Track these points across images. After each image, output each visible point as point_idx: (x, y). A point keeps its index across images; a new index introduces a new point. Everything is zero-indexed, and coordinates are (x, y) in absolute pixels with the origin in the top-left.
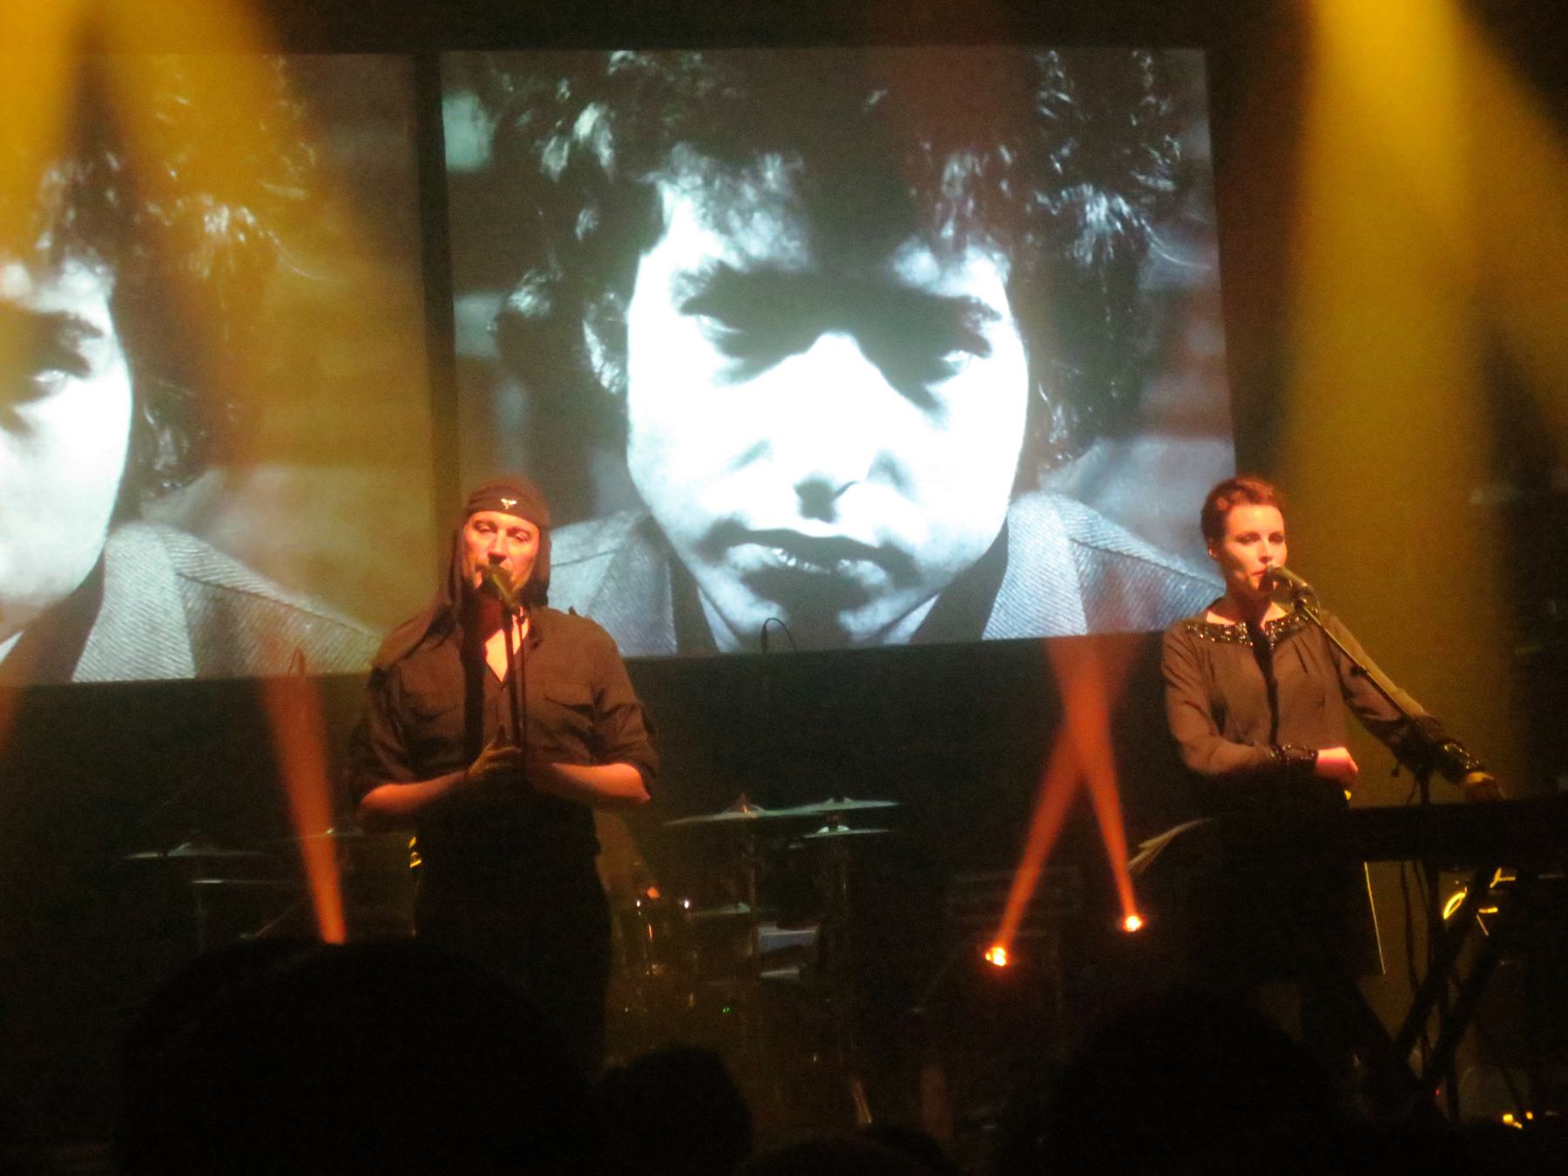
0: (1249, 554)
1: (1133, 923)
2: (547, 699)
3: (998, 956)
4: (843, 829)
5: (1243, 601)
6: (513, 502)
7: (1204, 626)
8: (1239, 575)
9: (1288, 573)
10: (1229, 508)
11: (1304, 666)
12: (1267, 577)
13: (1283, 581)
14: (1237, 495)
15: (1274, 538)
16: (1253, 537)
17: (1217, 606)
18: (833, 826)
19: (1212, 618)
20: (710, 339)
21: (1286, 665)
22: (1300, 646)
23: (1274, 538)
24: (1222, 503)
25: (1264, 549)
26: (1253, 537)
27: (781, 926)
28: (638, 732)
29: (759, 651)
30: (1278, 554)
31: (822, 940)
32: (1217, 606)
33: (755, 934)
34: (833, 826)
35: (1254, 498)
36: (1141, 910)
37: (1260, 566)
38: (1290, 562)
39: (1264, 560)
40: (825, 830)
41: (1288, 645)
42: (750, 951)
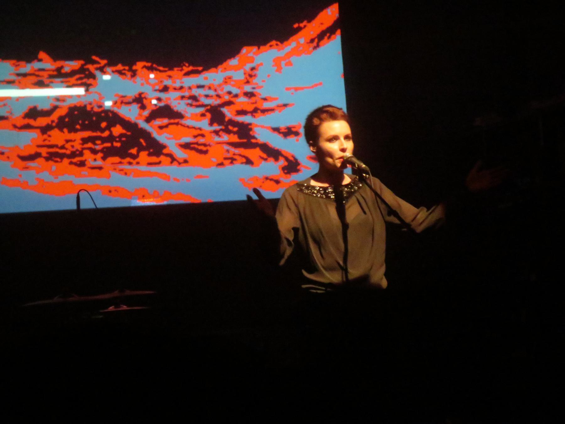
0: (334, 147)
4: (125, 307)
5: (329, 173)
7: (308, 187)
8: (330, 160)
9: (354, 160)
10: (320, 124)
11: (421, 223)
14: (324, 116)
15: (347, 137)
16: (334, 138)
17: (315, 177)
18: (117, 306)
19: (313, 183)
21: (353, 212)
22: (362, 201)
23: (347, 137)
24: (316, 121)
25: (342, 145)
26: (334, 138)
28: (289, 132)
30: (349, 145)
32: (315, 177)
34: (117, 306)
37: (342, 154)
38: (356, 152)
39: (343, 150)
40: (111, 308)
41: (353, 199)
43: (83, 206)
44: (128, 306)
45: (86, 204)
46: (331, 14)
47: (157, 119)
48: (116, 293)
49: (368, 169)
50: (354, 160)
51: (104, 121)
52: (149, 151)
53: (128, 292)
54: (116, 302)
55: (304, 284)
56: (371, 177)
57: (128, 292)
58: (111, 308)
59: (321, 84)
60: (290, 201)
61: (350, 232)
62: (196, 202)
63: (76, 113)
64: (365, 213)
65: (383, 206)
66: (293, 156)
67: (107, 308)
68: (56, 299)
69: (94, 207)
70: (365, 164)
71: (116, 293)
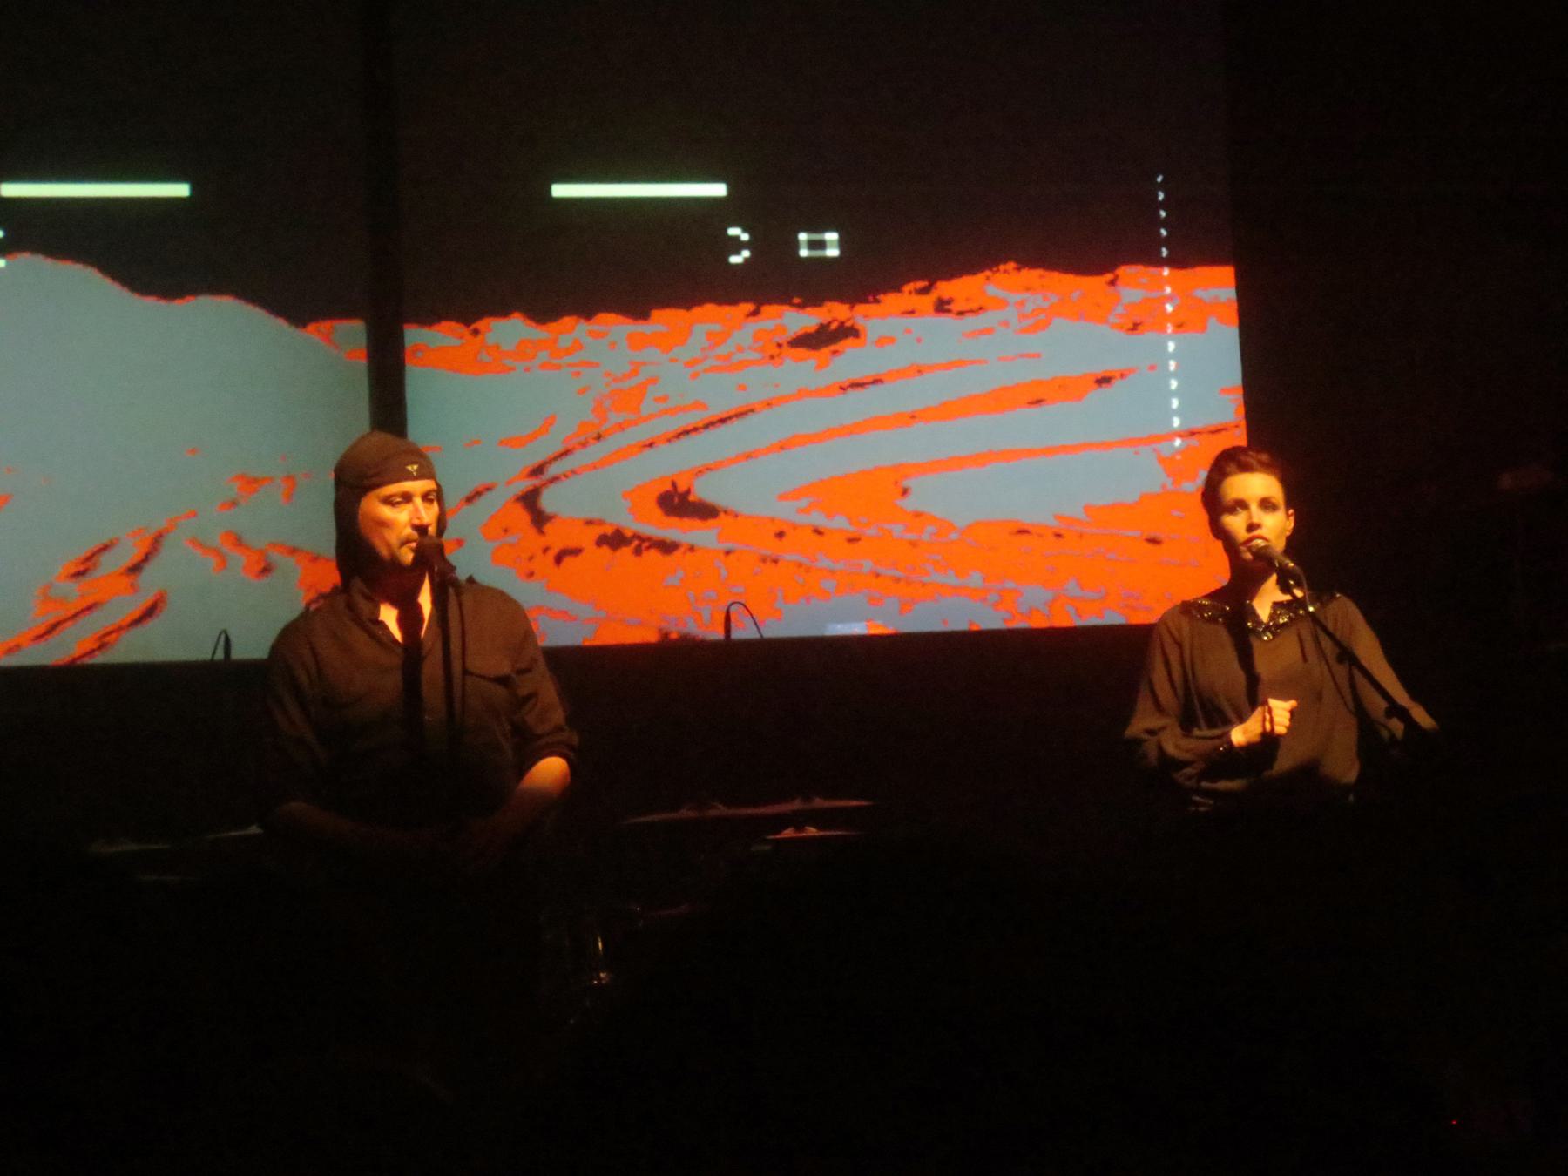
4: (811, 831)
18: (799, 828)
40: (789, 833)
43: (737, 634)
44: (820, 829)
45: (744, 631)
47: (445, 325)
48: (797, 805)
49: (1298, 570)
53: (819, 803)
54: (798, 820)
55: (1000, 725)
57: (819, 803)
58: (789, 833)
59: (1037, 356)
60: (1167, 639)
65: (1327, 644)
66: (1058, 517)
67: (779, 832)
68: (685, 813)
69: (757, 636)
71: (797, 805)
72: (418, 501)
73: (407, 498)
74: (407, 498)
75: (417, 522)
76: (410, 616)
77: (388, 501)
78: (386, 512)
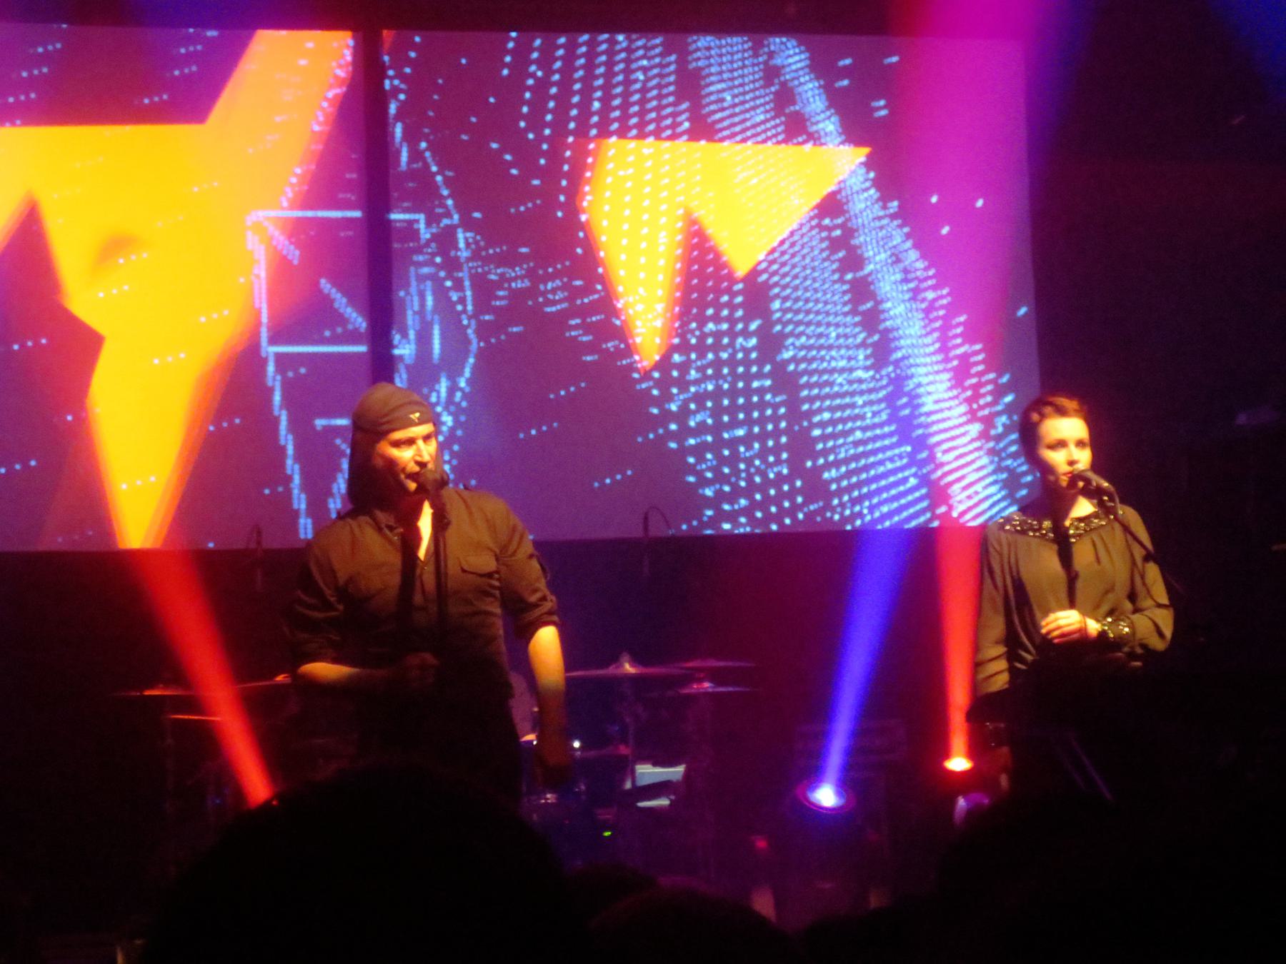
0: (1057, 458)
1: (826, 796)
2: (464, 571)
3: (826, 796)
6: (417, 415)
9: (1091, 475)
12: (1075, 477)
13: (1088, 481)
14: (1048, 410)
15: (1080, 444)
16: (1061, 444)
20: (842, 143)
23: (1080, 444)
24: (1035, 417)
25: (1070, 455)
26: (1061, 444)
27: (655, 764)
29: (637, 533)
30: (1084, 458)
31: (687, 774)
33: (633, 772)
35: (1062, 412)
36: (843, 786)
37: (1068, 469)
38: (1096, 466)
39: (1071, 463)
42: (628, 785)
46: (673, 797)
49: (1112, 489)
50: (1091, 475)
51: (456, 171)
52: (970, 405)
56: (1119, 505)
61: (1079, 584)
62: (848, 38)
63: (477, 215)
64: (1098, 560)
70: (1109, 481)
72: (420, 443)
73: (410, 442)
74: (410, 442)
75: (418, 459)
76: (411, 538)
77: (397, 444)
78: (395, 452)
